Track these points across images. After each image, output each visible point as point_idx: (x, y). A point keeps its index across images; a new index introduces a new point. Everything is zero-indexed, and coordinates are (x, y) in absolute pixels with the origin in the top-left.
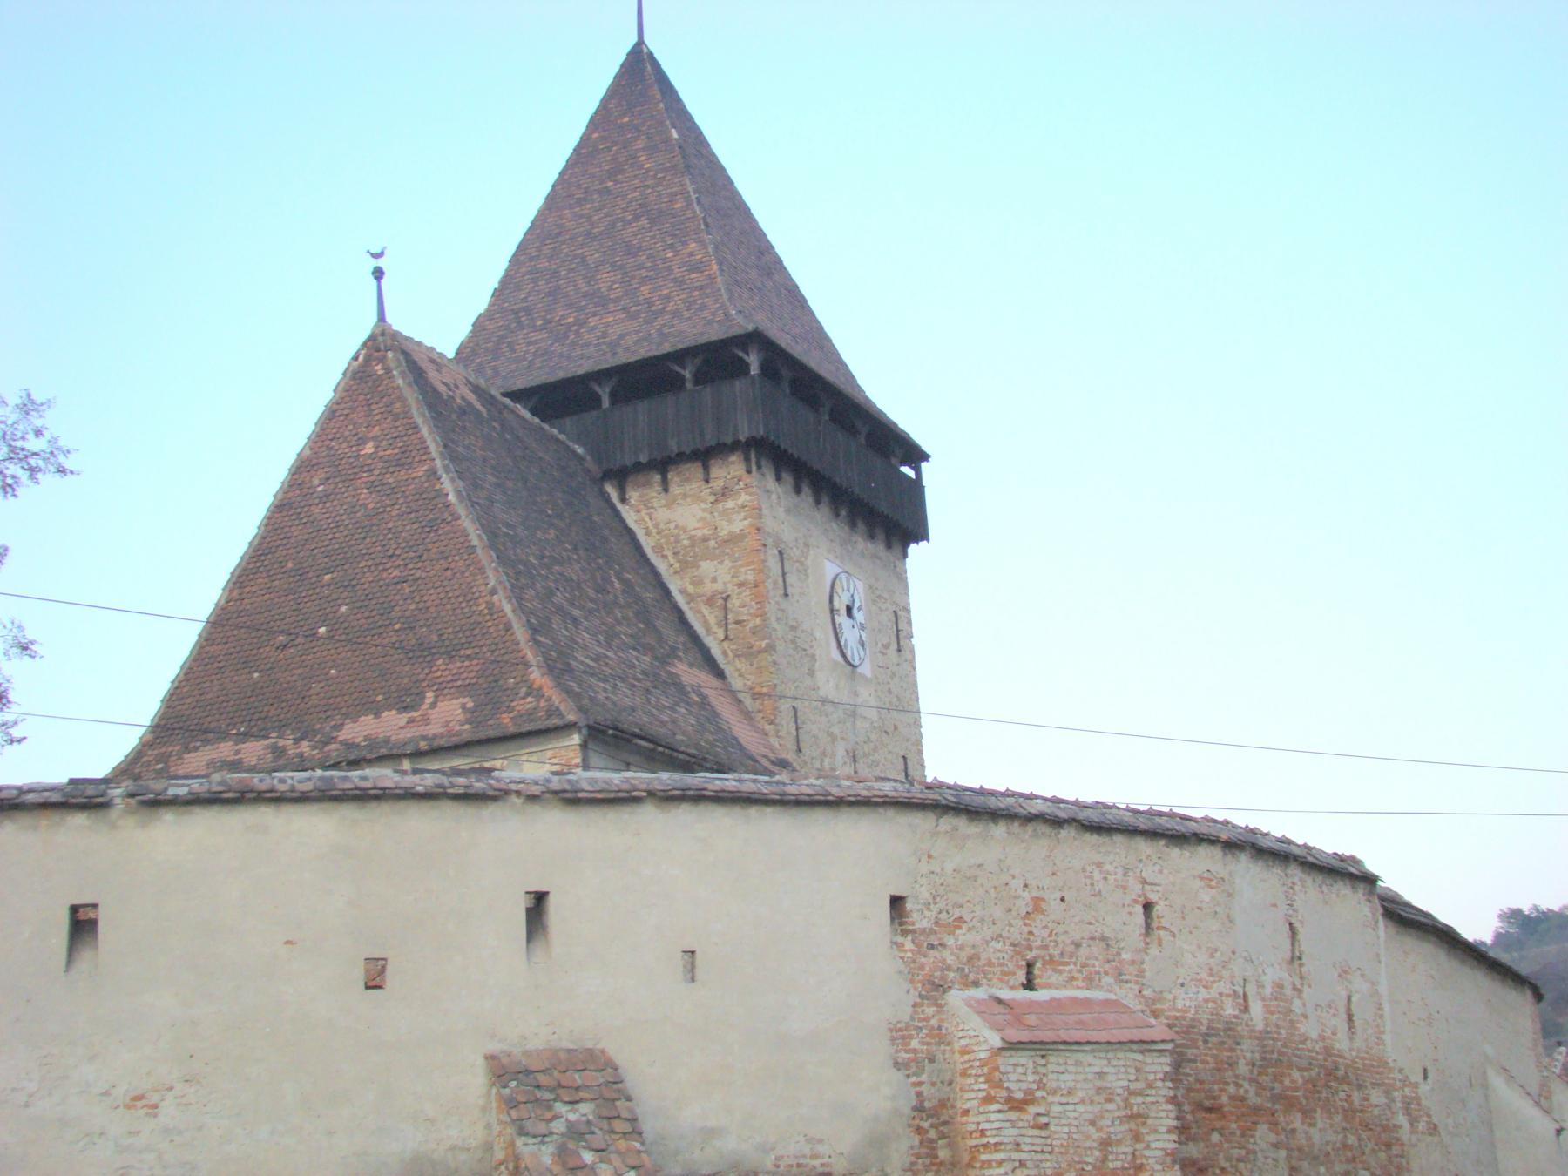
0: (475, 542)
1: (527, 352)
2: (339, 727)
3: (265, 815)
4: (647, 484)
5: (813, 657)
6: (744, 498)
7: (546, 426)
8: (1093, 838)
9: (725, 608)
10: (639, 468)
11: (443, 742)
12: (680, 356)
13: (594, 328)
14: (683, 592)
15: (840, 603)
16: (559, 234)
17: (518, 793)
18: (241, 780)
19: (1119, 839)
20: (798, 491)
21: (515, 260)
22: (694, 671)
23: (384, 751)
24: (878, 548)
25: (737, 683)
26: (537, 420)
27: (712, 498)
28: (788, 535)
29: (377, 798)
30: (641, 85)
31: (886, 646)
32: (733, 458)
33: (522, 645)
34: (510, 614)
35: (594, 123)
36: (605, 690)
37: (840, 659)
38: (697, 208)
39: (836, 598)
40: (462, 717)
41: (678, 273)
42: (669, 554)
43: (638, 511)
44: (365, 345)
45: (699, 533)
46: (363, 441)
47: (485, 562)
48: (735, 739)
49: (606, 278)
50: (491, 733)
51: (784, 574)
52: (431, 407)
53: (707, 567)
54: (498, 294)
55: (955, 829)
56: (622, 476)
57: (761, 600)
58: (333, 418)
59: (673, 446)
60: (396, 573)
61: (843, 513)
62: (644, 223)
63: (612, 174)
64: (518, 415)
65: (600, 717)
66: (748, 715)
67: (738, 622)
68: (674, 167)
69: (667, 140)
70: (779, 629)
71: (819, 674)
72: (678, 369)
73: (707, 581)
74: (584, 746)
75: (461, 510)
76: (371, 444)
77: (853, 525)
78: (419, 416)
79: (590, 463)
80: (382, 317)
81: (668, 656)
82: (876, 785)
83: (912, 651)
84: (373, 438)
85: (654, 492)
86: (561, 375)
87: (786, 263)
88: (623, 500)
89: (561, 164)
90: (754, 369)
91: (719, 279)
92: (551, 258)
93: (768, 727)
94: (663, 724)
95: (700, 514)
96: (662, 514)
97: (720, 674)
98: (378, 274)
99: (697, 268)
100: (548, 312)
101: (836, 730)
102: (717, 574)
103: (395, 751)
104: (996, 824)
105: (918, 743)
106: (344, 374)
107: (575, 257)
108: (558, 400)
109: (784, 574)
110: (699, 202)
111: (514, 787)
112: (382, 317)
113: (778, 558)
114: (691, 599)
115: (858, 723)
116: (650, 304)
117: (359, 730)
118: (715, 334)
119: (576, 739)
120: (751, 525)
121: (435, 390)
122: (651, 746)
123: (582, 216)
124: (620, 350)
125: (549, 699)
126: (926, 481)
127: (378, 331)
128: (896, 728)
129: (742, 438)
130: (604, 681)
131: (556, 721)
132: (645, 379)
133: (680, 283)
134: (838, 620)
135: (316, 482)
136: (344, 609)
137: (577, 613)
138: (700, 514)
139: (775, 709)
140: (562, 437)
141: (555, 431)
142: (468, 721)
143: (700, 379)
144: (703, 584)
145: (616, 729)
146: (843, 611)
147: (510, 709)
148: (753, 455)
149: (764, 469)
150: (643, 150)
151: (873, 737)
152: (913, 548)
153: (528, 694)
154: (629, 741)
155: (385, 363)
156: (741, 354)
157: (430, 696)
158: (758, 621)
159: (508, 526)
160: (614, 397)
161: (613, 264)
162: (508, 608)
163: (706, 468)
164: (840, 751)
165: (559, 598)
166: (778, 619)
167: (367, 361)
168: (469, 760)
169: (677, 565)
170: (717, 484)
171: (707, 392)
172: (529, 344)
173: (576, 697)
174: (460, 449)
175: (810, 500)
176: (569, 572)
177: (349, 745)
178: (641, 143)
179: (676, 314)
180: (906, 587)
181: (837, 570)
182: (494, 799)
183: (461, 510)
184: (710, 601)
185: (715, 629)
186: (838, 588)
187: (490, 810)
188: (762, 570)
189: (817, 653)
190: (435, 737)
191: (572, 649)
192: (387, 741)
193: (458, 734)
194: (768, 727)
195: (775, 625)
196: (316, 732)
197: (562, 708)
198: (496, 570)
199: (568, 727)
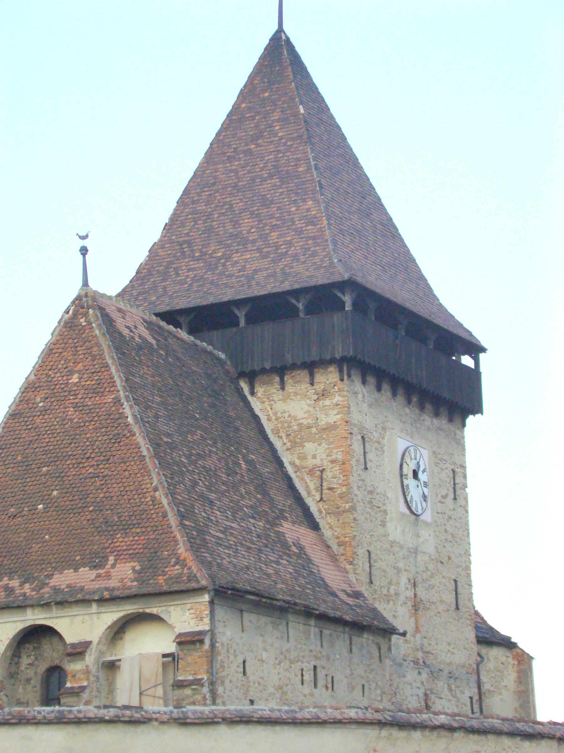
0: (145, 453)
1: (187, 276)
2: (50, 576)
3: (30, 731)
4: (269, 383)
5: (385, 512)
6: (337, 399)
7: (198, 342)
8: (475, 737)
9: (322, 478)
10: (264, 371)
11: (117, 593)
12: (296, 293)
13: (236, 262)
14: (292, 464)
15: (408, 470)
16: (214, 184)
17: (156, 720)
18: (20, 712)
19: (490, 737)
20: (379, 388)
21: (181, 202)
22: (296, 528)
23: (80, 596)
24: (443, 422)
25: (327, 533)
26: (192, 338)
27: (315, 397)
28: (369, 423)
29: (86, 723)
30: (280, 61)
31: (445, 497)
32: (332, 369)
33: (174, 528)
34: (166, 506)
35: (243, 95)
36: (229, 555)
37: (407, 511)
38: (315, 173)
39: (405, 466)
40: (131, 576)
41: (299, 224)
42: (283, 435)
43: (263, 402)
44: (73, 302)
45: (305, 422)
46: (71, 373)
47: (151, 467)
48: (322, 579)
49: (247, 223)
50: (150, 590)
51: (365, 453)
52: (118, 349)
53: (310, 447)
54: (168, 228)
55: (391, 735)
56: (252, 377)
57: (346, 473)
58: (51, 354)
59: (289, 359)
60: (91, 470)
61: (415, 399)
62: (276, 181)
63: (254, 139)
64: (178, 338)
65: (224, 580)
66: (334, 558)
67: (330, 489)
68: (300, 137)
69: (296, 114)
70: (359, 494)
71: (388, 524)
72: (294, 301)
73: (309, 457)
74: (212, 603)
75: (136, 429)
76: (76, 375)
77: (422, 408)
78: (110, 358)
79: (229, 365)
80: (85, 283)
81: (278, 518)
82: (346, 711)
83: (466, 499)
84: (79, 372)
85: (274, 390)
86: (211, 300)
87: (384, 201)
88: (253, 393)
89: (217, 127)
90: (348, 307)
91: (327, 232)
92: (208, 203)
93: (348, 567)
94: (268, 575)
95: (306, 408)
96: (280, 406)
97: (315, 526)
98: (84, 251)
99: (311, 222)
100: (203, 246)
101: (401, 565)
102: (316, 452)
103: (87, 597)
104: (415, 731)
105: (467, 568)
106: (59, 323)
107: (225, 204)
108: (205, 319)
109: (365, 453)
110: (316, 169)
111: (154, 716)
112: (85, 283)
113: (361, 442)
114: (298, 469)
115: (419, 557)
116: (277, 247)
117: (63, 579)
118: (321, 279)
119: (206, 598)
120: (342, 419)
121: (120, 334)
122: (257, 598)
123: (231, 171)
124: (253, 283)
125: (189, 568)
126: (482, 369)
127: (83, 293)
128: (449, 558)
129: (338, 356)
130: (228, 548)
131: (194, 585)
132: (270, 308)
133: (299, 232)
134: (406, 482)
135: (38, 400)
136: (55, 493)
137: (213, 496)
138: (306, 408)
139: (355, 553)
140: (210, 348)
141: (205, 344)
142: (136, 580)
143: (311, 310)
144: (305, 460)
145: (233, 589)
146: (411, 475)
147: (164, 573)
148: (345, 368)
149: (353, 377)
150: (279, 120)
151: (431, 567)
152: (470, 420)
153: (176, 564)
154: (243, 597)
155: (86, 303)
156: (339, 294)
157: (111, 559)
158: (344, 489)
159: (169, 435)
160: (250, 320)
161: (252, 213)
162: (165, 501)
163: (312, 375)
164: (404, 580)
165: (201, 488)
166: (359, 487)
167: (75, 315)
168: (136, 607)
169: (289, 444)
170: (319, 387)
171: (314, 320)
172: (189, 270)
173: (206, 564)
174: (137, 380)
175: (389, 394)
176: (209, 463)
177: (56, 590)
178: (276, 116)
179: (295, 257)
180: (464, 449)
181: (408, 444)
182: (144, 723)
183: (136, 429)
184: (311, 472)
185: (313, 492)
186: (407, 459)
187: (142, 728)
188: (349, 452)
189: (388, 508)
190: (114, 589)
191: (207, 526)
192: (82, 589)
193: (130, 588)
194: (348, 567)
195: (357, 492)
196: (35, 579)
197: (198, 575)
198: (158, 474)
199: (201, 590)
